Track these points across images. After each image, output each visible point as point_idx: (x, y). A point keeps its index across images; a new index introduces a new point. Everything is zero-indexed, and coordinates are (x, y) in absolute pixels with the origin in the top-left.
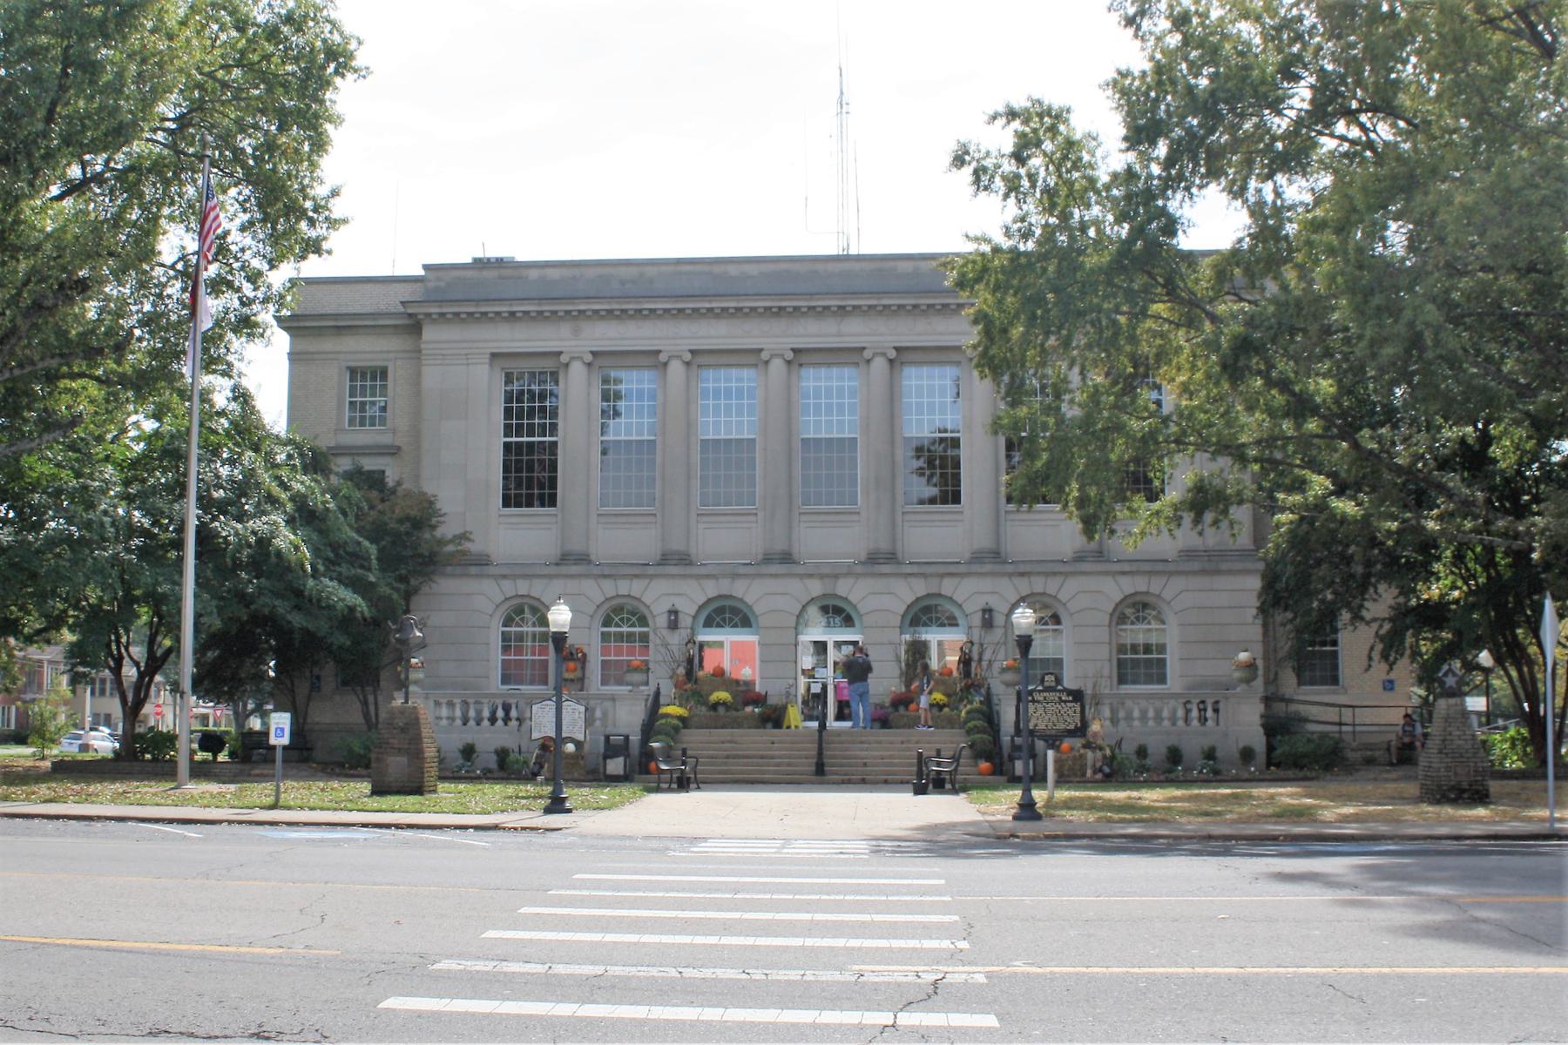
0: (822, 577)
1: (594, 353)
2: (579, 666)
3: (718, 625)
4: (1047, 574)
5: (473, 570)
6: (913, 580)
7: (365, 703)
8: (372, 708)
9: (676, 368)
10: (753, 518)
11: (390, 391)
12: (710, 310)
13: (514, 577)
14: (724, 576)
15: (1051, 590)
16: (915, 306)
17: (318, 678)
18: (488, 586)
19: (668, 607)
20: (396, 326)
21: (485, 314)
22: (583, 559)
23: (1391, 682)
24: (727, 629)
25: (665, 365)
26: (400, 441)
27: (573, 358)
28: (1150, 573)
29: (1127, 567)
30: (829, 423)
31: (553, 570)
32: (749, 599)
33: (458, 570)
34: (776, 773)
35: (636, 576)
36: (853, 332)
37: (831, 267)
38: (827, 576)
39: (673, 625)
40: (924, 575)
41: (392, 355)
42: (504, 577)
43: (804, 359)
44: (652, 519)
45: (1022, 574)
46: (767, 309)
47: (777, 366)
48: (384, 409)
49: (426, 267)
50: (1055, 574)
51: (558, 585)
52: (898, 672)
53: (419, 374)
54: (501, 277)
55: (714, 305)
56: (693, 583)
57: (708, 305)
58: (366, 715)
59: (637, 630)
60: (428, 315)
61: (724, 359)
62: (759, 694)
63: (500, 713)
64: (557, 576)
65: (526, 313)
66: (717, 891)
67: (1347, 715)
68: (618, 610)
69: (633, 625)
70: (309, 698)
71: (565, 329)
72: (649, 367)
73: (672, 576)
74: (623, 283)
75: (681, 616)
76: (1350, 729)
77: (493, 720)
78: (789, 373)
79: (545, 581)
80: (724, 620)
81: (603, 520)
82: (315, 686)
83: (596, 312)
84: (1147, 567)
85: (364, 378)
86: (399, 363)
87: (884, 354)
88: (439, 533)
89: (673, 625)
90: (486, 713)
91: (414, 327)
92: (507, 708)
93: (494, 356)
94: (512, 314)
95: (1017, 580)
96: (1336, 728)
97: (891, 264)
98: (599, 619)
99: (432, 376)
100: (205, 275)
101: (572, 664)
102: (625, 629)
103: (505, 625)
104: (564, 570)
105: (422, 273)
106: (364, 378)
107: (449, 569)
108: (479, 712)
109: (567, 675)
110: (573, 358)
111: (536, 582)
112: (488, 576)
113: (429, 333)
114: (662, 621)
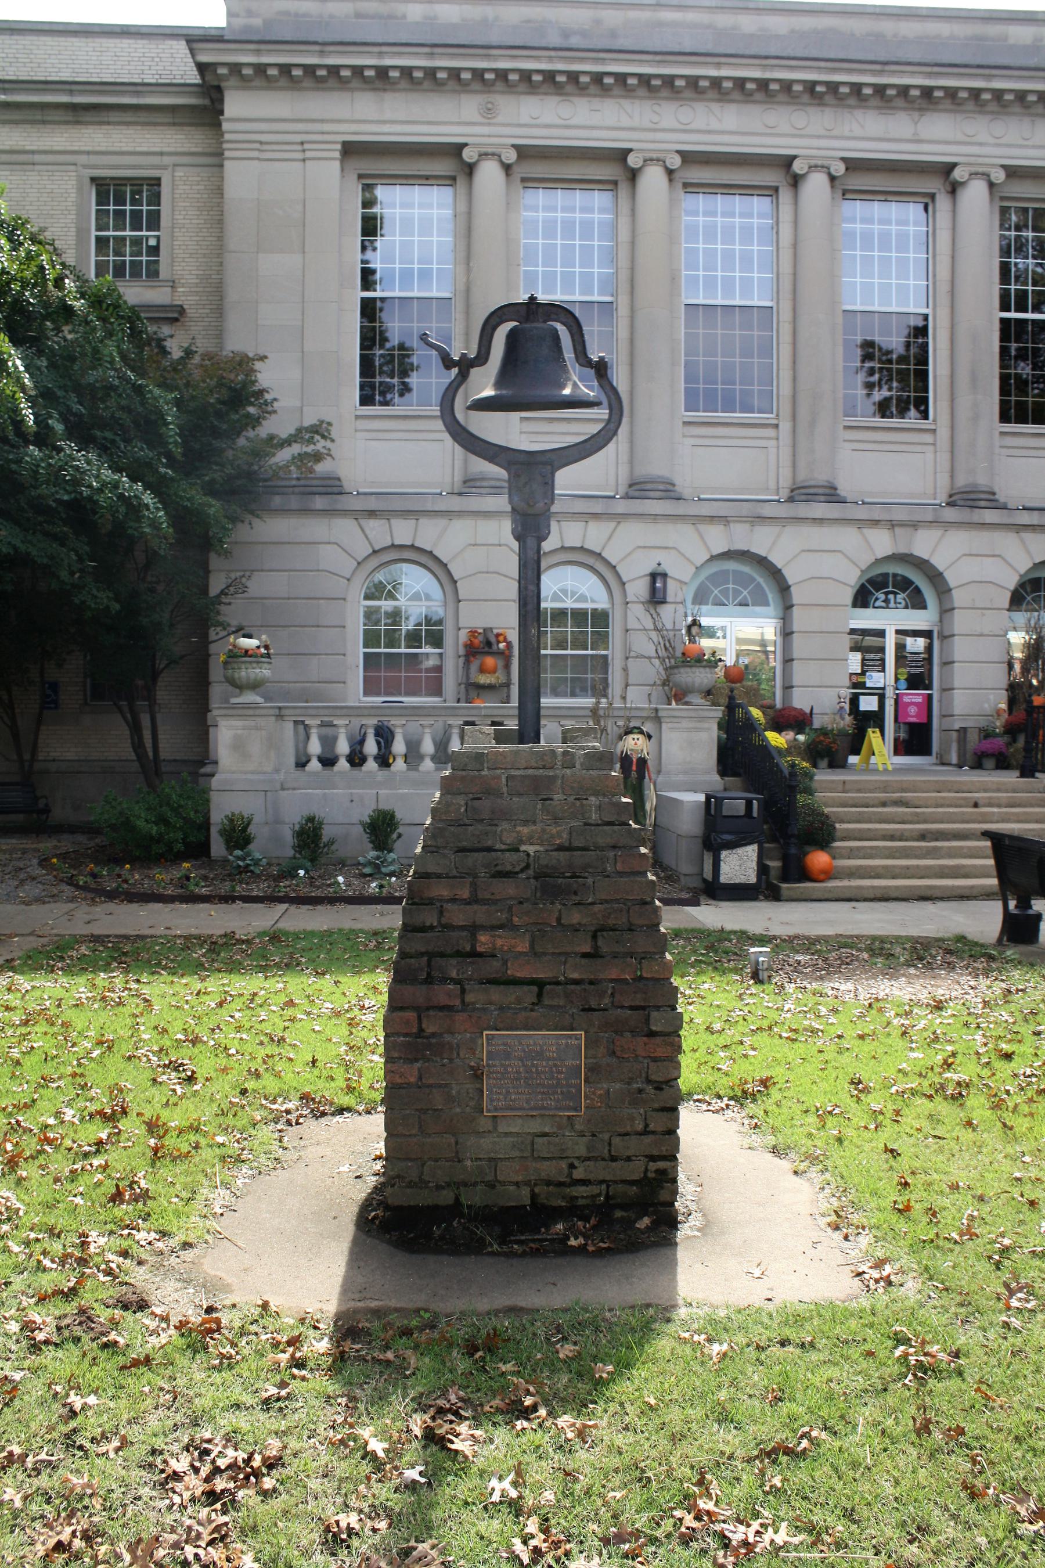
0: (892, 525)
2: (500, 663)
5: (319, 503)
7: (136, 728)
8: (147, 735)
11: (164, 221)
14: (741, 519)
17: (54, 687)
18: (344, 529)
19: (649, 567)
20: (173, 109)
21: (334, 70)
24: (731, 608)
26: (183, 297)
27: (484, 155)
30: (885, 289)
31: (456, 503)
33: (294, 502)
35: (596, 516)
36: (936, 137)
38: (902, 524)
39: (656, 598)
41: (167, 160)
42: (372, 514)
48: (155, 250)
52: (1004, 683)
53: (219, 191)
54: (358, 15)
56: (687, 530)
58: (138, 746)
60: (236, 68)
62: (801, 712)
63: (371, 747)
64: (461, 514)
65: (407, 72)
70: (39, 722)
73: (655, 517)
74: (566, 34)
75: (669, 581)
77: (328, 762)
80: (725, 592)
82: (50, 698)
85: (120, 200)
86: (179, 173)
88: (269, 427)
89: (656, 598)
90: (343, 747)
91: (203, 104)
92: (385, 736)
94: (382, 72)
97: (994, 30)
99: (241, 177)
100: (10, 1243)
101: (490, 661)
103: (367, 597)
104: (474, 503)
106: (120, 200)
107: (277, 501)
108: (329, 742)
109: (484, 679)
110: (484, 155)
112: (345, 513)
113: (237, 105)
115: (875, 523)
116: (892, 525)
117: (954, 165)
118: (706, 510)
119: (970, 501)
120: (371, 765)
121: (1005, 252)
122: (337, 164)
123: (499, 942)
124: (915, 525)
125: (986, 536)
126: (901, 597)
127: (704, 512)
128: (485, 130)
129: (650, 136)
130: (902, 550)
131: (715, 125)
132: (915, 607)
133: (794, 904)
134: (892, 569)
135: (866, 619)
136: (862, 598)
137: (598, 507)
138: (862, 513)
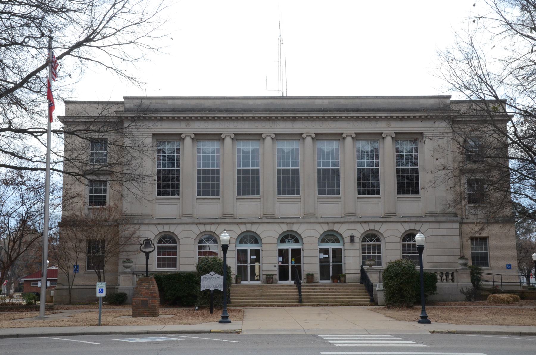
1: (195, 134)
3: (245, 243)
4: (375, 222)
6: (322, 225)
9: (228, 141)
10: (259, 200)
12: (242, 118)
13: (163, 224)
15: (213, 230)
16: (323, 117)
22: (272, 216)
23: (510, 265)
24: (330, 244)
25: (224, 139)
27: (307, 136)
28: (415, 222)
29: (406, 220)
32: (258, 233)
34: (259, 302)
37: (240, 101)
40: (328, 223)
43: (239, 138)
44: (218, 201)
45: (365, 222)
46: (265, 117)
47: (309, 140)
49: (125, 98)
50: (378, 222)
51: (222, 227)
55: (244, 115)
57: (241, 116)
59: (172, 245)
60: (126, 118)
61: (251, 138)
65: (167, 118)
66: (422, 348)
67: (497, 278)
68: (164, 237)
69: (170, 243)
71: (183, 125)
72: (216, 140)
76: (500, 284)
77: (447, 273)
78: (233, 144)
79: (176, 226)
81: (198, 201)
83: (196, 118)
84: (414, 219)
87: (351, 136)
93: (154, 135)
95: (364, 225)
96: (492, 283)
98: (197, 241)
102: (167, 245)
105: (123, 100)
111: (336, 225)
114: (347, 240)
115: (283, 223)
116: (287, 223)
117: (302, 134)
118: (240, 221)
119: (308, 218)
120: (444, 272)
121: (358, 158)
122: (151, 139)
123: (3, 324)
124: (293, 223)
125: (312, 225)
126: (292, 240)
127: (407, 220)
128: (187, 130)
129: (227, 130)
130: (331, 229)
131: (243, 127)
132: (296, 243)
133: (282, 309)
134: (330, 233)
135: (325, 246)
136: (282, 241)
137: (214, 221)
138: (279, 221)
